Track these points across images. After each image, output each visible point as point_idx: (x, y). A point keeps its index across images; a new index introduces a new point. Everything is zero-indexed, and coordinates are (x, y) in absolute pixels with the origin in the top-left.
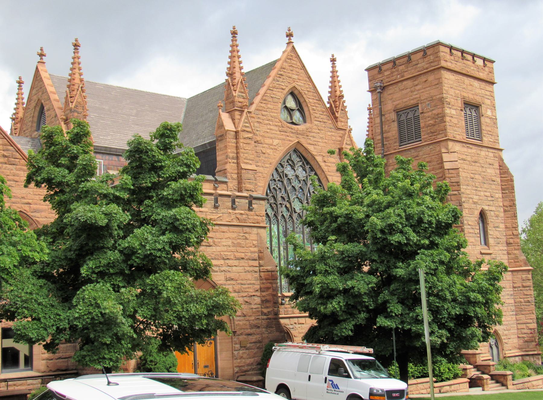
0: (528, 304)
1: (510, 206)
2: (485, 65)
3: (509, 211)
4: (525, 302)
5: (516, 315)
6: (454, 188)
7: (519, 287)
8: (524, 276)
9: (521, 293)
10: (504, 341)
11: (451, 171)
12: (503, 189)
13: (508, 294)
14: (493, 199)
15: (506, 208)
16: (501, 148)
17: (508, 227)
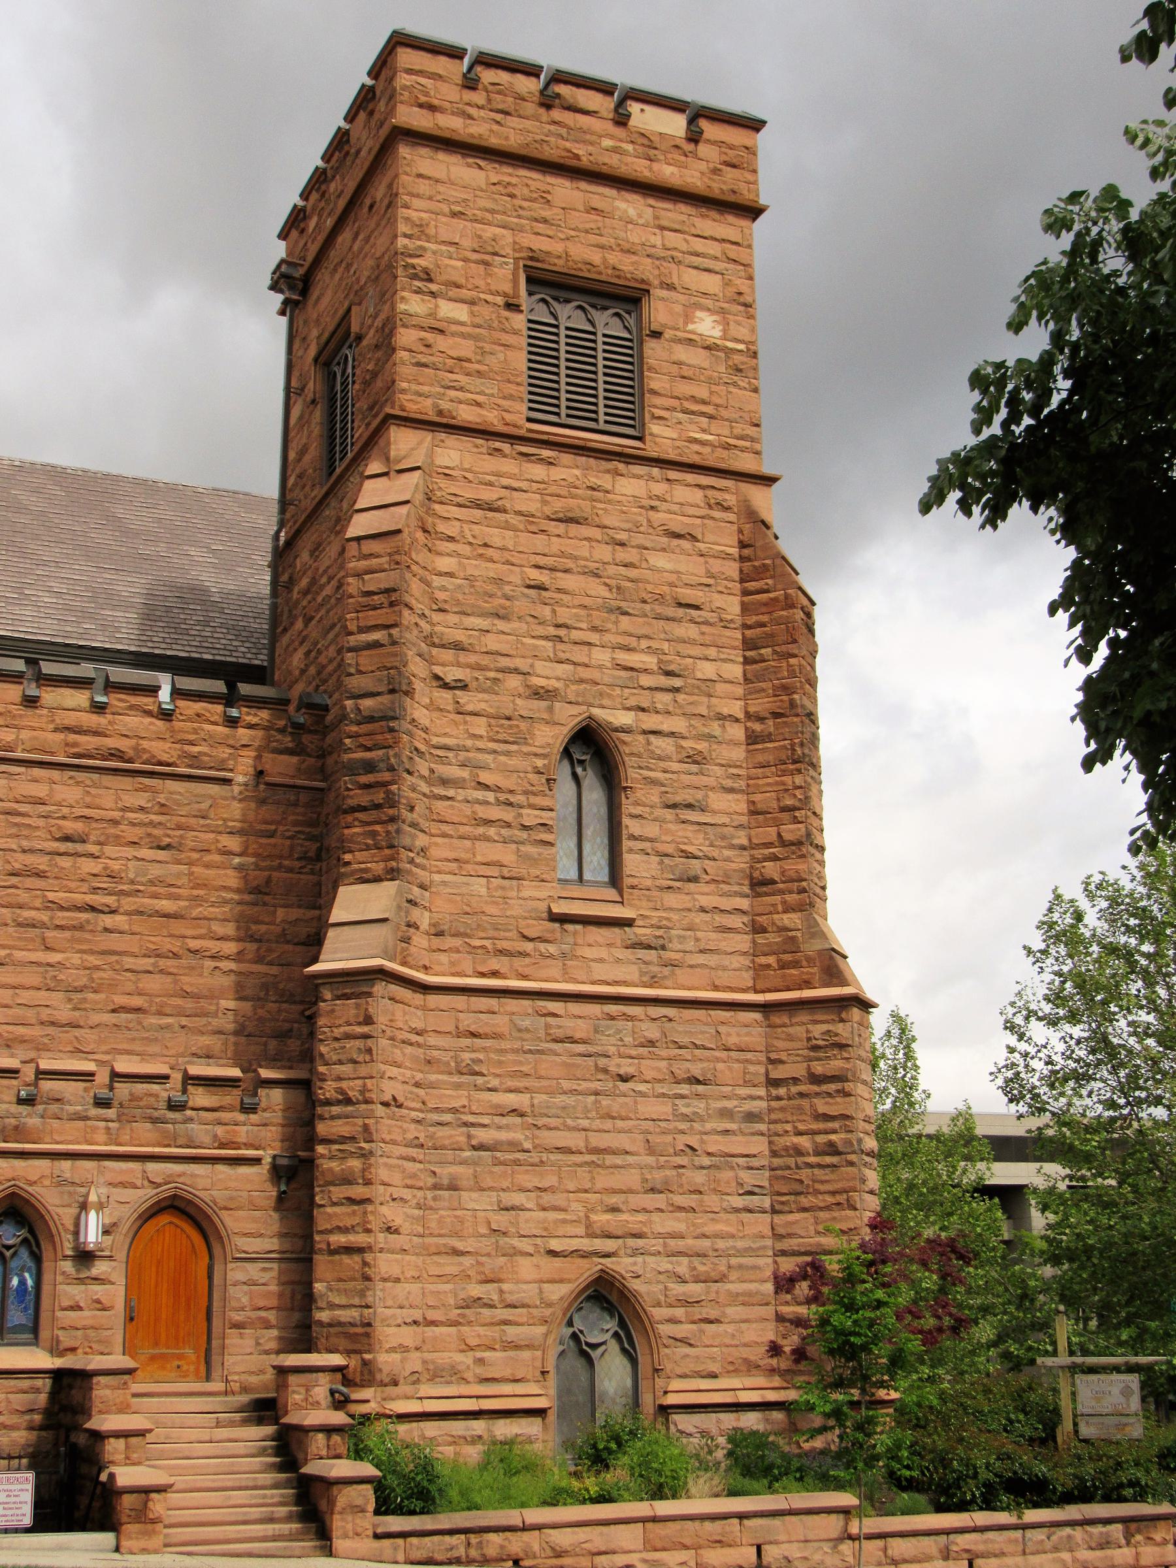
0: (828, 1160)
1: (776, 715)
2: (694, 137)
3: (769, 738)
4: (817, 1153)
5: (774, 1211)
6: (373, 617)
7: (795, 1080)
8: (818, 1030)
9: (800, 1108)
10: (665, 1329)
11: (369, 547)
12: (748, 644)
13: (726, 1114)
14: (677, 682)
15: (757, 727)
16: (767, 470)
17: (760, 806)
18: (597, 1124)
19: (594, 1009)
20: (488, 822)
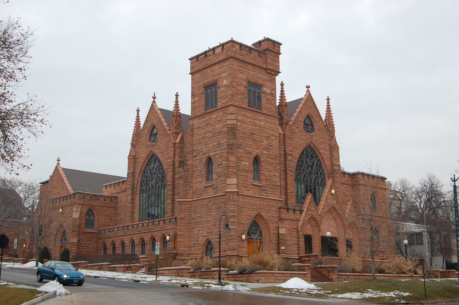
18: (208, 217)
19: (208, 200)
20: (198, 175)
